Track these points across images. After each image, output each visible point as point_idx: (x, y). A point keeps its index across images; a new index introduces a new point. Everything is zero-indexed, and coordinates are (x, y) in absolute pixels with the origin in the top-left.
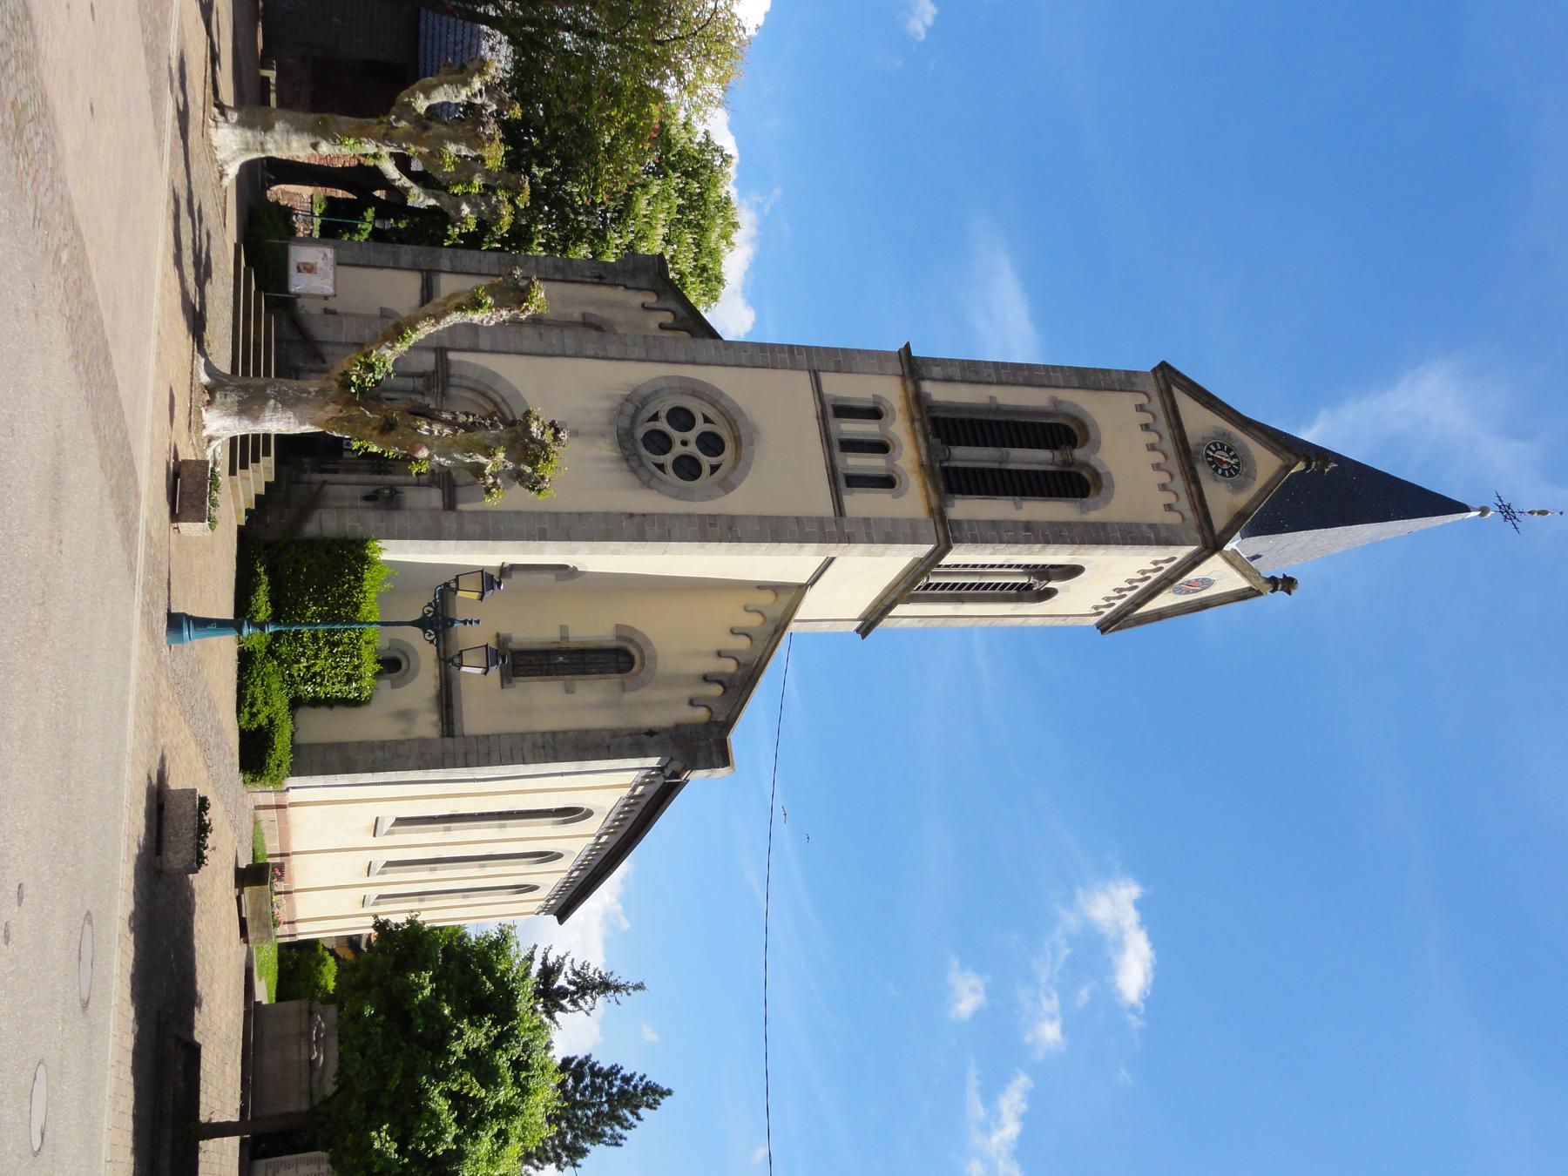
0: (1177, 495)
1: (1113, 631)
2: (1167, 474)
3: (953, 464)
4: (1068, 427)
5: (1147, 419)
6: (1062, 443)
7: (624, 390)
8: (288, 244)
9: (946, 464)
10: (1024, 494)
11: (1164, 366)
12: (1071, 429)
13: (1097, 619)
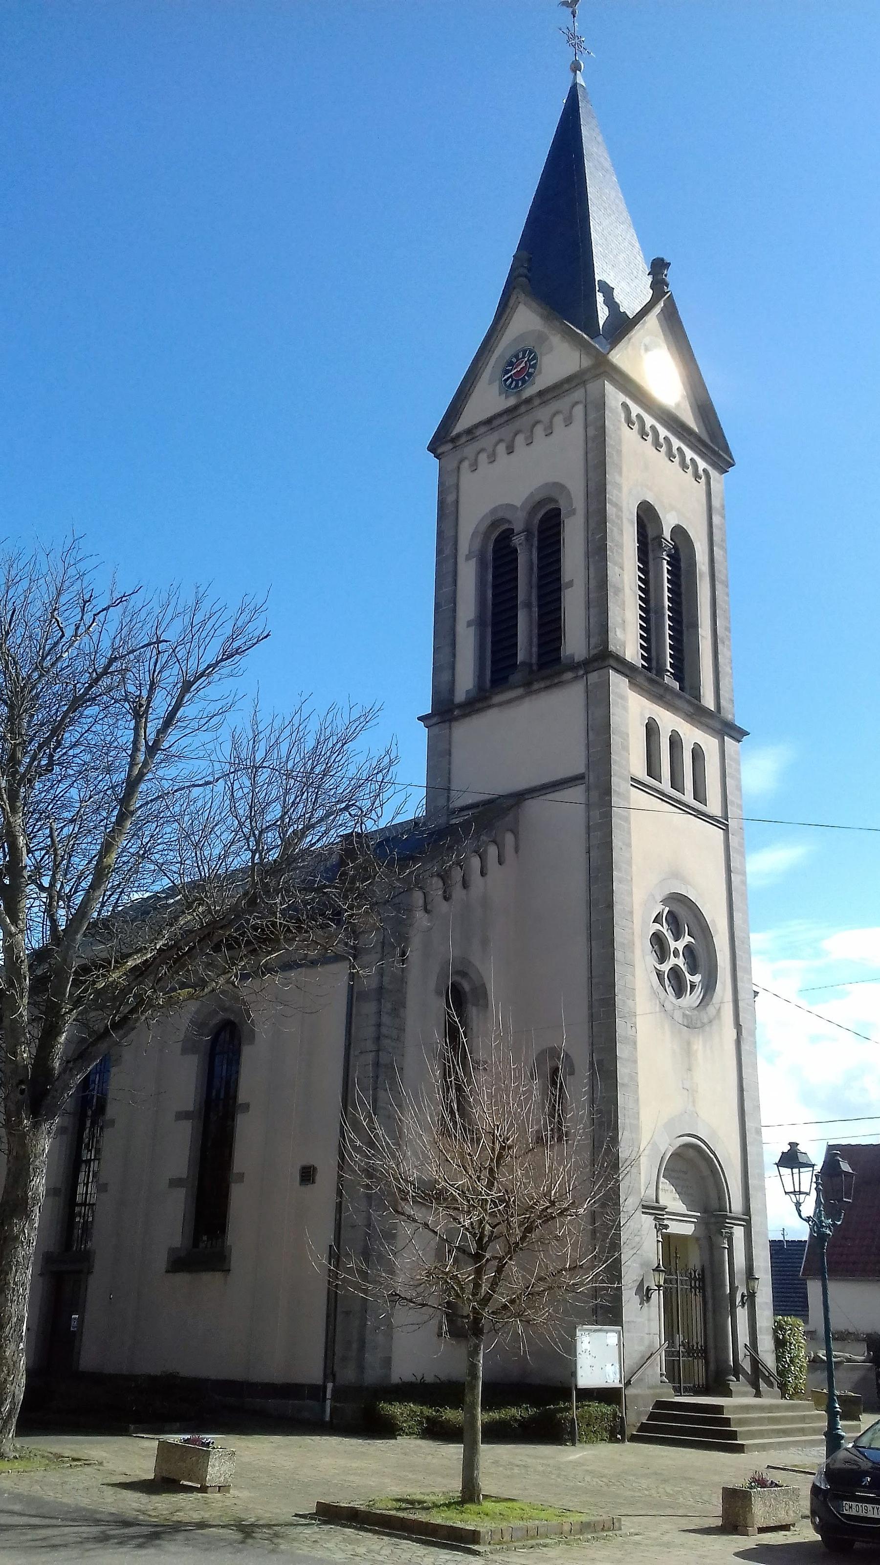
0: (554, 415)
1: (731, 457)
2: (574, 408)
3: (534, 660)
4: (496, 540)
5: (501, 448)
6: (509, 546)
7: (656, 1004)
8: (577, 1389)
9: (535, 668)
10: (559, 579)
11: (432, 448)
12: (499, 535)
13: (713, 473)
